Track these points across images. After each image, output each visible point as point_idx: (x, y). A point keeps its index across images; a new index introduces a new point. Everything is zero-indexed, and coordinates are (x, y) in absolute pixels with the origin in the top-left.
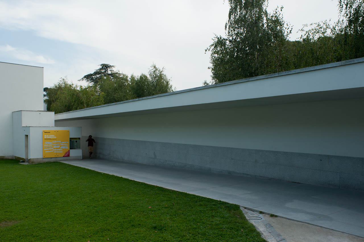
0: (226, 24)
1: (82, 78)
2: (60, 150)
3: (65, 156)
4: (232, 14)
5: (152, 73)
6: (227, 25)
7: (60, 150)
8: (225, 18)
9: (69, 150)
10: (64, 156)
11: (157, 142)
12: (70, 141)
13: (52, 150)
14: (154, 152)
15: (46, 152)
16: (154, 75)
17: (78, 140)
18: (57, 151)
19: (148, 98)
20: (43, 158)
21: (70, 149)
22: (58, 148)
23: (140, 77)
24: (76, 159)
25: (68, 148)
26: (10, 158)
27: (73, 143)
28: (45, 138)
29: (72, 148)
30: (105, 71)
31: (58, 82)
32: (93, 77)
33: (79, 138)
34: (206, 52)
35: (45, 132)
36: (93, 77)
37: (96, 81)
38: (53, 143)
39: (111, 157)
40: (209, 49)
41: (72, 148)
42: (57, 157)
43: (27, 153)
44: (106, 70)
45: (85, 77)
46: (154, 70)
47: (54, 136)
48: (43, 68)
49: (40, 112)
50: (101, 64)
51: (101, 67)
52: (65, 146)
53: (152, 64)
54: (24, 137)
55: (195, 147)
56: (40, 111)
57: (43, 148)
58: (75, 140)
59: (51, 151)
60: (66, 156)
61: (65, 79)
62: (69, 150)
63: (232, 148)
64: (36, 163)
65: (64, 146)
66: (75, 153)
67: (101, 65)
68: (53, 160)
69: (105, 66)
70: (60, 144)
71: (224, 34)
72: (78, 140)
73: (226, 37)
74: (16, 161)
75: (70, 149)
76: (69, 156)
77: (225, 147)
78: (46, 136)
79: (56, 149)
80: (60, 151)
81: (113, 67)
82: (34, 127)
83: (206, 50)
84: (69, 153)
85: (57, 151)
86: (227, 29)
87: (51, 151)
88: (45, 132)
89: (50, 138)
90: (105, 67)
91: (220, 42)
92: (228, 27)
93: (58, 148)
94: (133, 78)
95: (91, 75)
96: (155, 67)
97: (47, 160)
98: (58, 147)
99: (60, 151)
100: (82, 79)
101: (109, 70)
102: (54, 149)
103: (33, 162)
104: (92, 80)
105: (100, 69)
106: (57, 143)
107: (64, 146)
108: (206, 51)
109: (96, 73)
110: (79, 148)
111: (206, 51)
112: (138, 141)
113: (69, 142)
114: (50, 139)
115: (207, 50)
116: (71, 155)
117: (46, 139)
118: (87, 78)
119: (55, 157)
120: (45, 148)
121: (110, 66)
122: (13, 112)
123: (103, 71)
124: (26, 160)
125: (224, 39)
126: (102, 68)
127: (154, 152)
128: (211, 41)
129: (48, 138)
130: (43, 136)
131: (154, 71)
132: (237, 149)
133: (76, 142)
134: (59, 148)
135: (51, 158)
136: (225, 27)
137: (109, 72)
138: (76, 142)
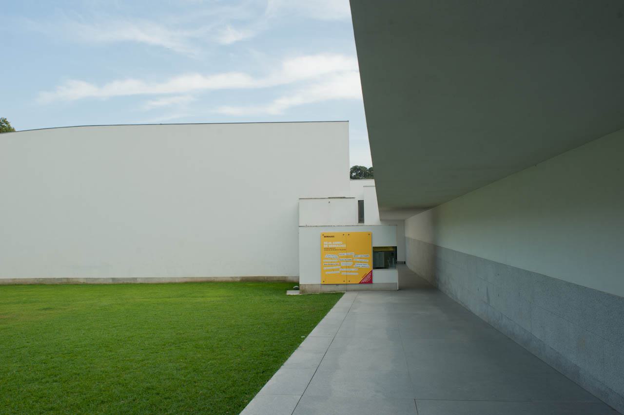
2: (353, 270)
3: (363, 283)
7: (353, 270)
9: (371, 272)
10: (360, 283)
13: (336, 270)
20: (321, 284)
21: (375, 267)
22: (349, 267)
28: (326, 246)
35: (325, 237)
48: (348, 121)
49: (330, 200)
60: (365, 283)
62: (371, 272)
65: (361, 262)
66: (386, 277)
76: (370, 282)
78: (328, 244)
84: (371, 276)
88: (325, 237)
93: (349, 267)
98: (350, 263)
103: (303, 292)
106: (347, 257)
114: (334, 249)
116: (374, 281)
117: (327, 249)
119: (344, 283)
129: (330, 246)
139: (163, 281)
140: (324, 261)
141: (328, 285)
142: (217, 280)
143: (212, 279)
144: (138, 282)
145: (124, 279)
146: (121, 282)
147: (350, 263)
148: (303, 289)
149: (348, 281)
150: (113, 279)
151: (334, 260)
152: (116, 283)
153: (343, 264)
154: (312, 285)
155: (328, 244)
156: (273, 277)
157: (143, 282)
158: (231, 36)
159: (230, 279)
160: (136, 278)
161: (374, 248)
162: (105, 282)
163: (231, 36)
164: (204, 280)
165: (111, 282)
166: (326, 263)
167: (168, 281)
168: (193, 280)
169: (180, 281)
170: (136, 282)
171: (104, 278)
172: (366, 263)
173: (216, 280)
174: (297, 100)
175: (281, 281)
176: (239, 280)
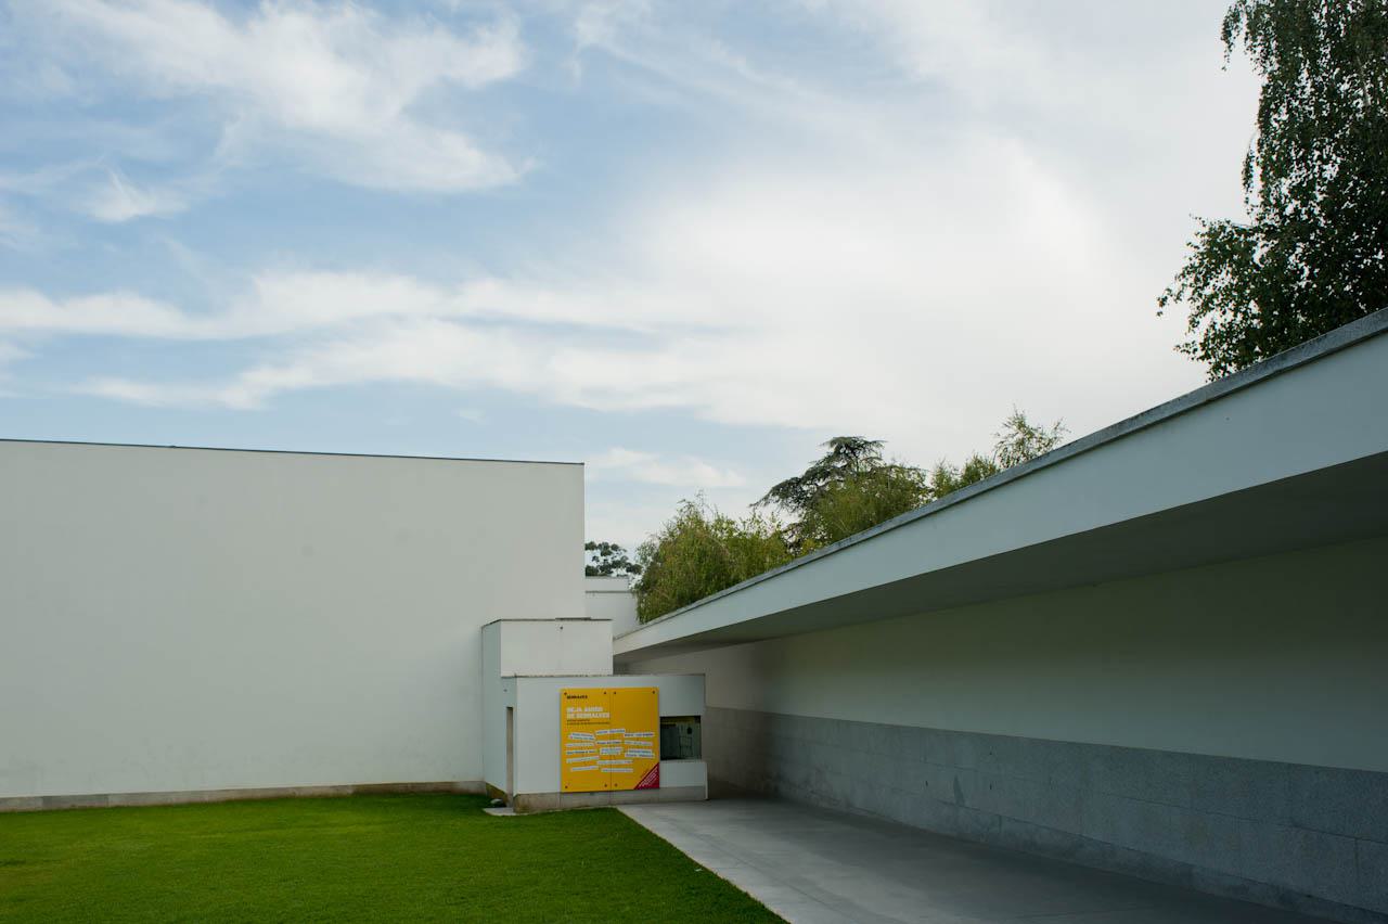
0: (1249, 158)
1: (764, 495)
2: (623, 762)
3: (642, 788)
4: (1276, 111)
5: (1010, 449)
6: (1253, 164)
7: (623, 762)
8: (1245, 135)
9: (658, 765)
10: (637, 788)
11: (961, 734)
12: (662, 727)
13: (592, 763)
14: (956, 780)
15: (573, 769)
16: (1022, 459)
17: (693, 725)
18: (611, 766)
19: (870, 535)
20: (561, 793)
21: (663, 758)
22: (615, 758)
23: (968, 469)
24: (685, 799)
25: (653, 755)
26: (473, 789)
27: (675, 737)
28: (570, 716)
29: (667, 754)
30: (849, 465)
31: (675, 517)
32: (805, 488)
33: (698, 718)
34: (1163, 309)
35: (569, 697)
36: (805, 488)
37: (810, 503)
38: (598, 738)
39: (812, 792)
40: (1175, 291)
41: (667, 754)
42: (614, 788)
43: (511, 779)
44: (850, 458)
45: (776, 490)
46: (1020, 436)
47: (601, 709)
48: (583, 464)
49: (561, 623)
50: (830, 438)
51: (832, 450)
52: (634, 747)
53: (1012, 414)
54: (505, 710)
55: (1118, 757)
56: (562, 619)
57: (563, 757)
58: (686, 725)
59: (590, 768)
60: (646, 787)
61: (697, 501)
62: (658, 765)
63: (1290, 765)
64: (538, 812)
65: (638, 747)
66: (681, 775)
67: (832, 443)
68: (597, 801)
69: (847, 446)
70: (623, 739)
71: (1239, 208)
72: (693, 725)
73: (1248, 222)
74: (481, 799)
75: (663, 758)
76: (656, 785)
77: (1171, 750)
78: (574, 712)
79: (611, 757)
80: (626, 766)
81: (874, 448)
82: (532, 677)
83: (1165, 299)
84: (658, 774)
85: (611, 766)
86: (1257, 183)
87: (590, 768)
88: (569, 697)
89: (586, 716)
90: (848, 447)
91: (1222, 248)
92: (1257, 171)
93: (615, 758)
94: (941, 476)
95: (798, 481)
96: (1021, 425)
97: (575, 802)
98: (618, 750)
99: (626, 766)
100: (766, 498)
101: (861, 456)
102: (601, 758)
103: (525, 808)
104: (801, 498)
105: (829, 459)
106: (612, 737)
107: (638, 747)
108: (1163, 302)
109: (812, 475)
110: (699, 756)
111: (1163, 302)
112: (895, 730)
113: (656, 734)
114: (586, 722)
115: (1170, 300)
116: (663, 783)
117: (573, 722)
118: (784, 496)
119: (605, 789)
120: (570, 755)
121: (866, 443)
122: (483, 628)
123: (840, 465)
124: (510, 799)
125: (1240, 231)
126: (837, 452)
127: (956, 780)
128: (1183, 249)
129: (579, 716)
130: (563, 713)
131: (1021, 443)
132: (1318, 770)
133: (690, 731)
134: (621, 757)
135: (592, 793)
136: (1244, 176)
137: (865, 467)
138: (690, 731)
139: (174, 800)
140: (569, 745)
141: (582, 795)
142: (302, 794)
143: (290, 792)
144: (110, 805)
145: (74, 798)
146: (66, 806)
147: (618, 750)
148: (526, 803)
149: (613, 784)
150: (46, 799)
151: (588, 745)
152: (54, 808)
153: (604, 751)
154: (542, 795)
155: (574, 712)
156: (426, 784)
157: (126, 804)
158: (122, 204)
159: (331, 792)
160: (106, 796)
161: (662, 719)
162: (25, 807)
163: (122, 204)
164: (271, 794)
165: (40, 805)
166: (571, 749)
167: (184, 799)
168: (245, 795)
169: (214, 798)
170: (104, 804)
171: (21, 799)
172: (646, 748)
173: (297, 793)
174: (297, 377)
175: (443, 791)
176: (350, 791)
